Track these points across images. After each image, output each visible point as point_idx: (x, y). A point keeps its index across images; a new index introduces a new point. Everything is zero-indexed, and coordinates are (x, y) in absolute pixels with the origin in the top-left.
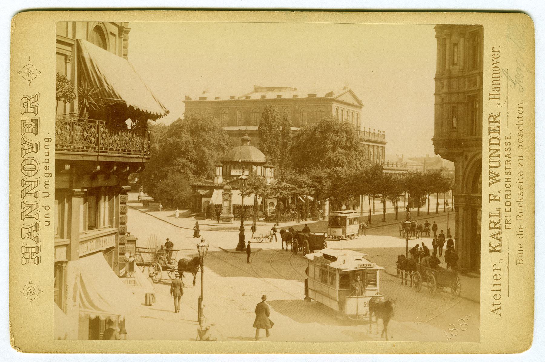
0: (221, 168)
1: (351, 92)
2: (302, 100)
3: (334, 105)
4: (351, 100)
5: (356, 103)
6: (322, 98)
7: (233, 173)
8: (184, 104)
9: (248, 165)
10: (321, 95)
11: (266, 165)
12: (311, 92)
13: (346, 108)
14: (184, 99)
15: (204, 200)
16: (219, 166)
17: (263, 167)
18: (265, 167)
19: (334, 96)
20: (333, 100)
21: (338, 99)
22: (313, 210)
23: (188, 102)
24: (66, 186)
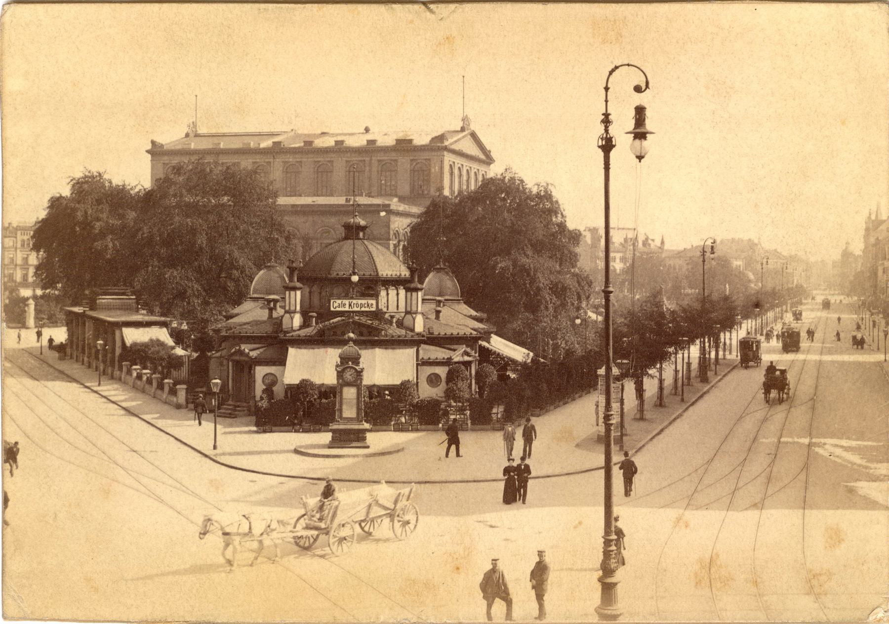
0: (299, 293)
1: (474, 135)
2: (385, 150)
3: (448, 158)
4: (474, 151)
5: (482, 157)
6: (423, 146)
7: (337, 305)
8: (149, 156)
9: (371, 285)
10: (422, 140)
11: (412, 285)
12: (400, 136)
13: (467, 164)
14: (149, 147)
15: (260, 372)
16: (294, 289)
17: (402, 292)
18: (408, 290)
19: (446, 143)
20: (446, 149)
21: (454, 147)
22: (459, 397)
23: (156, 151)
24: (409, 317)
